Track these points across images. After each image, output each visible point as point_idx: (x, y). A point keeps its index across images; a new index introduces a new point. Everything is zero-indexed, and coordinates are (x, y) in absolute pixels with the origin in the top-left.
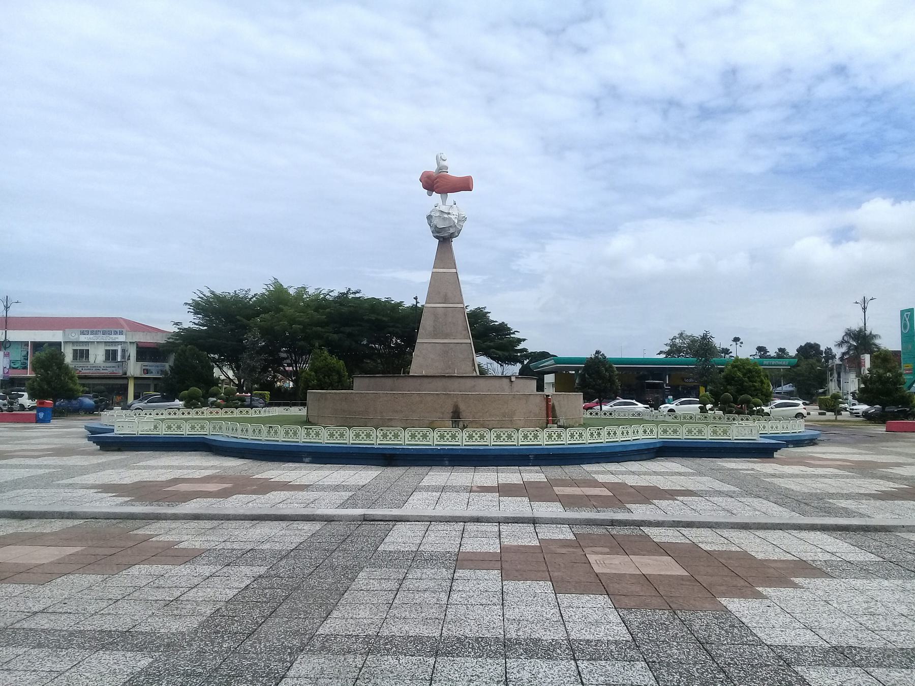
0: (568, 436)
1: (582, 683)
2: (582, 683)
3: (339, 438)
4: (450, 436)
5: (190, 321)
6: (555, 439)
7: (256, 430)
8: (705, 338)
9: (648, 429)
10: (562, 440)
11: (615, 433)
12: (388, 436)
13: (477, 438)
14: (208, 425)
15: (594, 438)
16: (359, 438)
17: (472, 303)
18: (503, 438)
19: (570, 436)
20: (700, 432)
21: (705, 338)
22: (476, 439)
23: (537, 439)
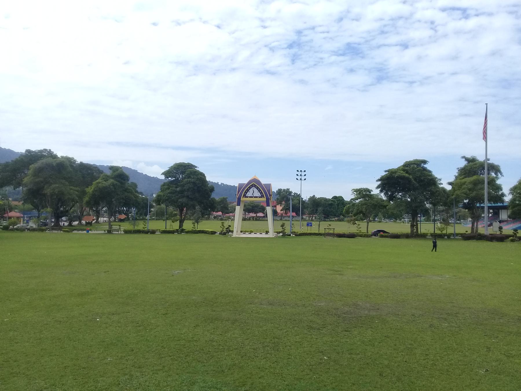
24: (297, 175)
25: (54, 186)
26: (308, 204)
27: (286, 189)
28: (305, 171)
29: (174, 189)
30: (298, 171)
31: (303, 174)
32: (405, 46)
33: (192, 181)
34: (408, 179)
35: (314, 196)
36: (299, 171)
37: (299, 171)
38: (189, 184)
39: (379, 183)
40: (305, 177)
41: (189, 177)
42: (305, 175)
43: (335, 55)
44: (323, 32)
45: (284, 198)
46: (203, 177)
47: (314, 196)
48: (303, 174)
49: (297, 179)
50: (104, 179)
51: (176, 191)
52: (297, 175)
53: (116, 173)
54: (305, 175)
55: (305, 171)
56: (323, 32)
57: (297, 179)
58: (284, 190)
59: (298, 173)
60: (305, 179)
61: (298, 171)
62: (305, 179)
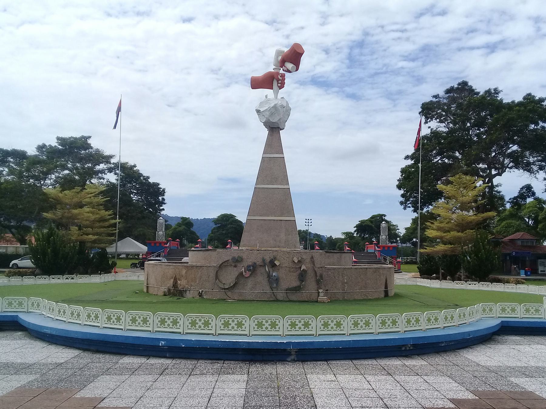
0: (378, 323)
1: (388, 407)
2: (388, 407)
3: (202, 328)
4: (230, 324)
5: (54, 143)
6: (139, 323)
7: (34, 303)
8: (413, 219)
9: (488, 308)
10: (397, 326)
11: (417, 321)
12: (166, 322)
13: (533, 311)
14: (26, 302)
15: (431, 324)
16: (228, 328)
17: (301, 226)
18: (301, 324)
19: (406, 322)
20: (513, 310)
21: (413, 219)
22: (508, 312)
23: (147, 324)
24: (306, 222)
25: (139, 229)
26: (326, 244)
27: (305, 230)
28: (311, 220)
29: (221, 231)
30: (306, 219)
31: (310, 221)
32: (492, 48)
33: (234, 227)
34: (371, 226)
35: (331, 236)
36: (307, 219)
37: (307, 219)
38: (232, 229)
39: (355, 229)
40: (311, 224)
41: (232, 224)
42: (311, 222)
43: (405, 60)
44: (397, 31)
45: (304, 239)
46: (241, 224)
47: (331, 236)
48: (310, 221)
49: (306, 225)
50: (178, 225)
51: (223, 233)
52: (306, 222)
53: (185, 222)
54: (311, 222)
55: (311, 220)
56: (397, 31)
57: (306, 225)
58: (304, 231)
59: (306, 221)
60: (311, 225)
61: (306, 219)
62: (311, 225)
